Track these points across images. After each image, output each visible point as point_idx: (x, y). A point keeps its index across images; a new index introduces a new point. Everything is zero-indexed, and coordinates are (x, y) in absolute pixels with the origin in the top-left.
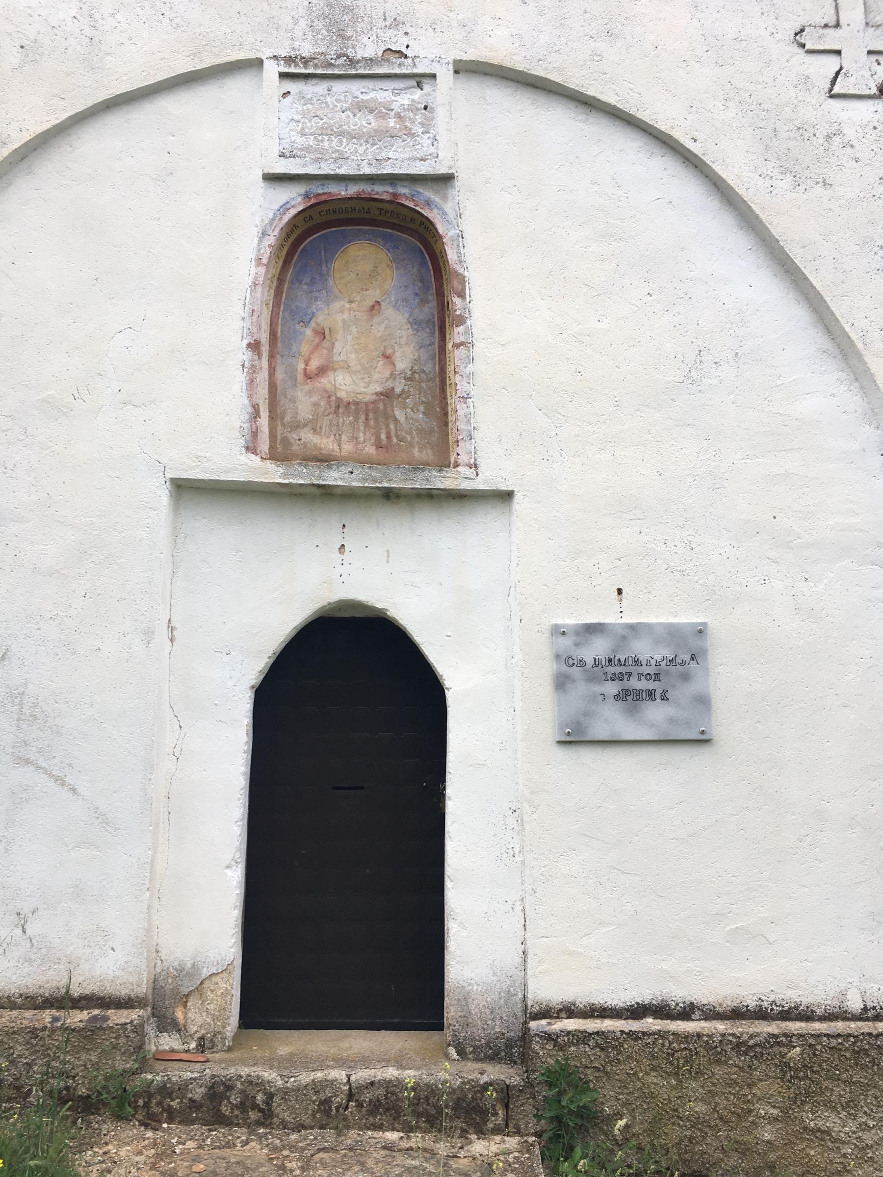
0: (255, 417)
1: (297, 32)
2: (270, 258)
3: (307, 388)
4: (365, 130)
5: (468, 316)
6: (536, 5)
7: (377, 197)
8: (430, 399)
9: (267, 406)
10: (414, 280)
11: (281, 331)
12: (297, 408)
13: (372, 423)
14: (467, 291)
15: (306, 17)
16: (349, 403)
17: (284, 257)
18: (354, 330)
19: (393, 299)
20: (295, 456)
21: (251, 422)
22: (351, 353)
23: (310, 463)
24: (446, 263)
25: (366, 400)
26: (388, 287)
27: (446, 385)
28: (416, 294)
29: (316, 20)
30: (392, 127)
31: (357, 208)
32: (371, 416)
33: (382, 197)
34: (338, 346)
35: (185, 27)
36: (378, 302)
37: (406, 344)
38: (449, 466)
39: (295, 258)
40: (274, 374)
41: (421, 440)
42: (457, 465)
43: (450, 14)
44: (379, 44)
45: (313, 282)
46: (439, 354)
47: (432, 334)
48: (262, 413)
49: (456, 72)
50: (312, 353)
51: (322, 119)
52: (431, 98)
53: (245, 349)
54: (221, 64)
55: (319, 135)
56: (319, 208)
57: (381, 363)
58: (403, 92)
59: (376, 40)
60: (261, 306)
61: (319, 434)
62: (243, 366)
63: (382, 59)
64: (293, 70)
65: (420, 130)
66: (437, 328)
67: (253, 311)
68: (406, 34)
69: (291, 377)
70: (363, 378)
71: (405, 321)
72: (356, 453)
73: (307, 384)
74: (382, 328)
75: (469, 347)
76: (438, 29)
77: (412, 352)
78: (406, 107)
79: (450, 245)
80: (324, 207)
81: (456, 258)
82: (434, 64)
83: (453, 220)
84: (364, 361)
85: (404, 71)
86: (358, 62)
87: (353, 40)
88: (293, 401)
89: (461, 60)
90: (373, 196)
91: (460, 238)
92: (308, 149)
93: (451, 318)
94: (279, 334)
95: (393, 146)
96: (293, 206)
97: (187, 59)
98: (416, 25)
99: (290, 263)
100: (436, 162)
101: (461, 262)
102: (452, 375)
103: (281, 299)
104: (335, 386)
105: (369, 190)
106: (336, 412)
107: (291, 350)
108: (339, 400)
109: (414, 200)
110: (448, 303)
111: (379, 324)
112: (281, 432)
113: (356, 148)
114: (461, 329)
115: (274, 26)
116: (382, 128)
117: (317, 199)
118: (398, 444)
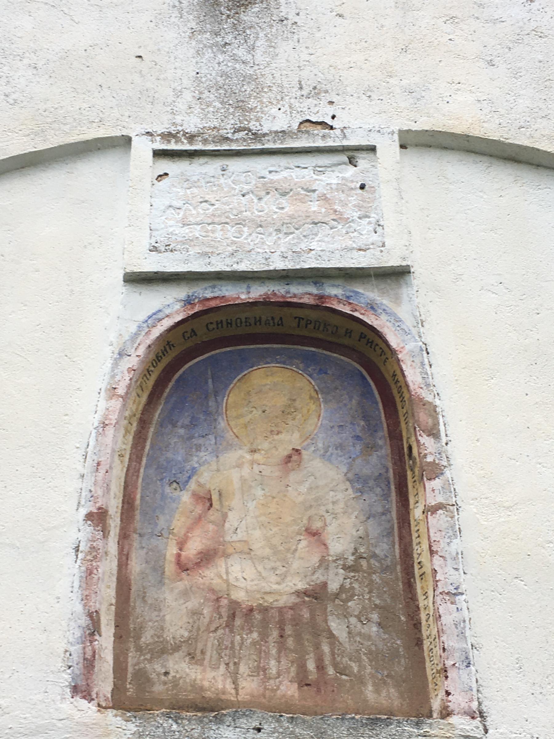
0: (92, 634)
1: (180, 105)
2: (129, 387)
3: (181, 585)
4: (275, 217)
5: (445, 464)
6: (509, 66)
7: (295, 300)
8: (389, 600)
9: (112, 617)
10: (353, 417)
11: (142, 497)
12: (163, 620)
13: (290, 642)
14: (442, 427)
15: (192, 89)
16: (251, 610)
17: (150, 388)
18: (259, 492)
19: (320, 445)
20: (158, 703)
21: (83, 642)
22: (254, 529)
23: (184, 714)
24: (404, 390)
25: (281, 604)
26: (313, 428)
27: (414, 577)
28: (358, 438)
29: (206, 91)
30: (314, 212)
31: (264, 318)
32: (289, 630)
33: (301, 301)
34: (233, 519)
35: (25, 103)
36: (297, 450)
37: (344, 513)
38: (430, 716)
39: (167, 390)
40: (127, 564)
41: (377, 671)
42: (446, 713)
43: (391, 81)
44: (294, 115)
45: (193, 424)
46: (400, 528)
47: (386, 496)
48: (103, 628)
49: (402, 147)
50: (190, 529)
51: (213, 205)
52: (370, 175)
53: (82, 522)
54: (73, 143)
55: (209, 224)
56: (206, 319)
57: (303, 543)
58: (329, 169)
59: (289, 110)
60: (112, 456)
61: (200, 662)
62: (77, 549)
63: (299, 131)
64: (173, 146)
65: (356, 215)
66: (393, 487)
67: (99, 464)
68: (331, 103)
69: (154, 569)
70: (274, 569)
71: (341, 477)
72: (264, 697)
73: (181, 580)
74: (303, 489)
75: (452, 512)
76: (374, 96)
77: (355, 526)
78: (334, 186)
79: (409, 363)
80: (214, 318)
81: (419, 379)
82: (372, 134)
83: (411, 328)
84: (276, 541)
85: (330, 143)
86: (265, 135)
87: (258, 112)
88: (157, 607)
89: (409, 131)
90: (289, 300)
91: (425, 352)
92: (189, 241)
93: (417, 470)
94: (138, 502)
95: (316, 235)
96: (167, 316)
97: (25, 139)
98: (344, 93)
99: (159, 398)
100: (382, 251)
101: (428, 385)
102: (425, 558)
103: (143, 448)
104: (227, 581)
105: (283, 291)
106: (229, 625)
107: (156, 525)
108: (234, 605)
109: (350, 304)
110: (410, 448)
111: (300, 483)
112: (135, 660)
113: (262, 239)
114: (436, 483)
115: (148, 100)
116: (300, 213)
117: (204, 305)
118: (336, 679)
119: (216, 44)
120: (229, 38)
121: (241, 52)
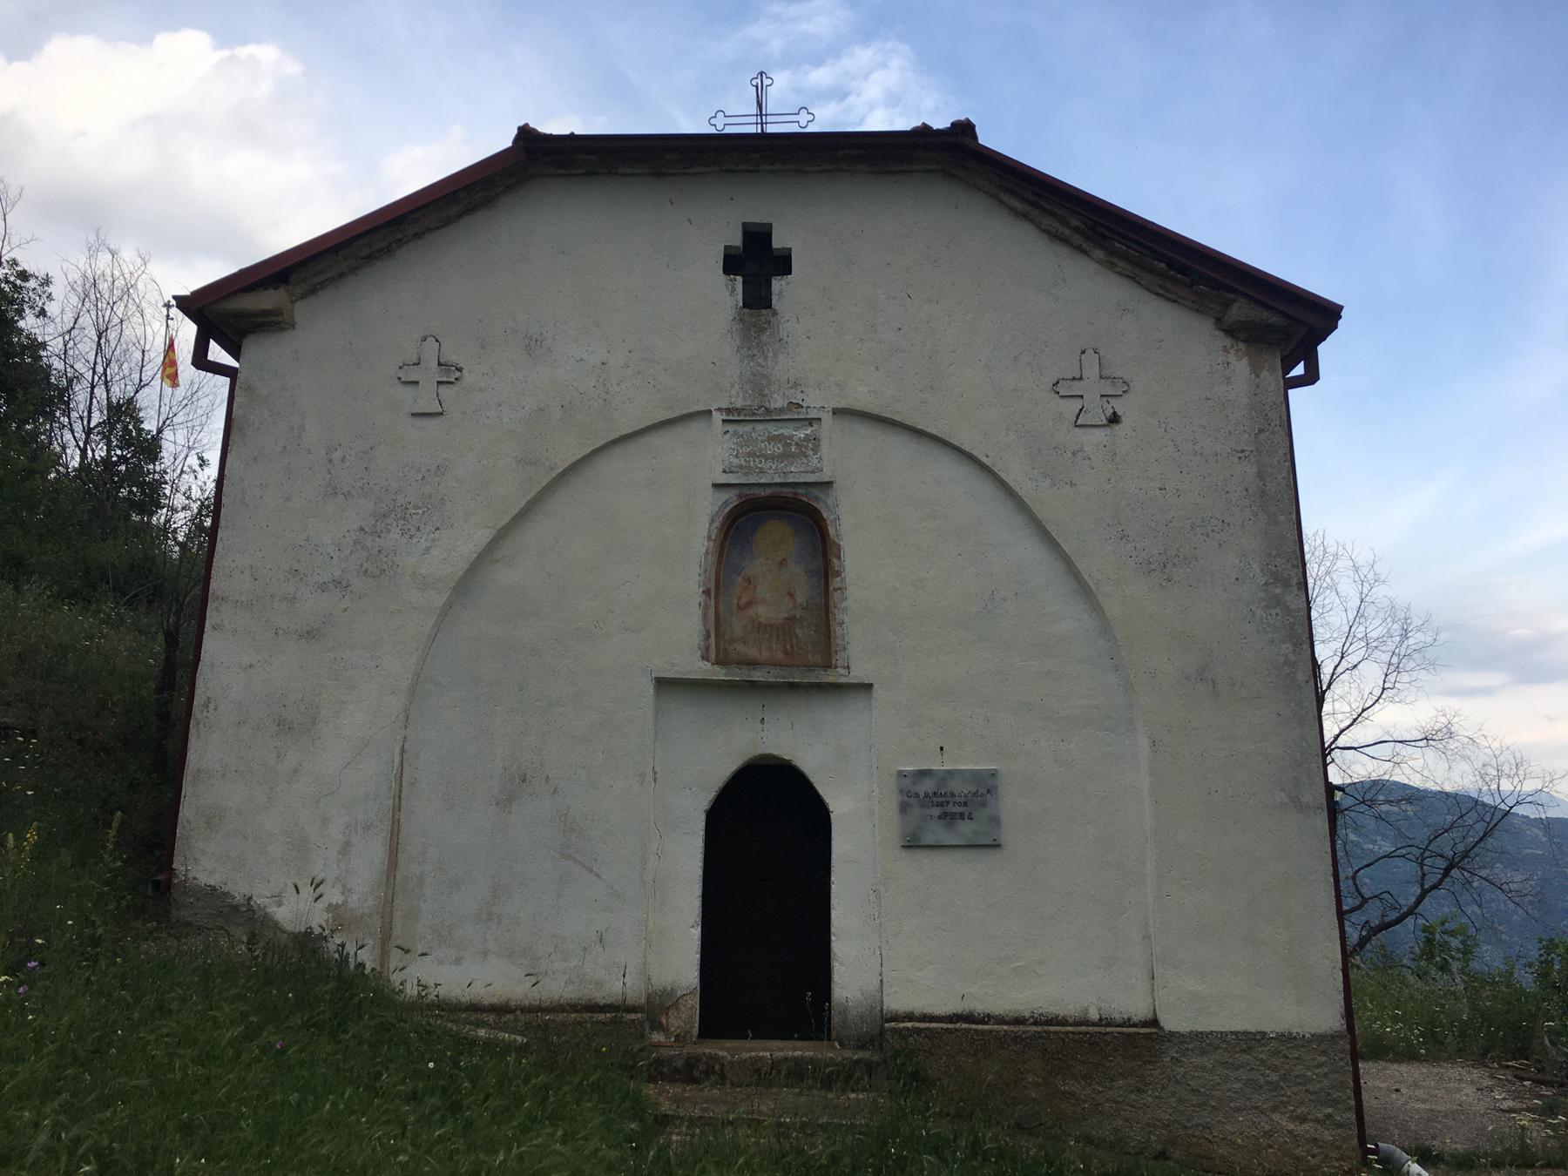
13: (781, 638)
38: (830, 667)
42: (836, 667)
57: (787, 599)
62: (700, 604)
68: (802, 392)
101: (838, 536)
106: (758, 631)
108: (760, 623)
114: (838, 579)
119: (749, 355)
120: (755, 352)
121: (761, 360)
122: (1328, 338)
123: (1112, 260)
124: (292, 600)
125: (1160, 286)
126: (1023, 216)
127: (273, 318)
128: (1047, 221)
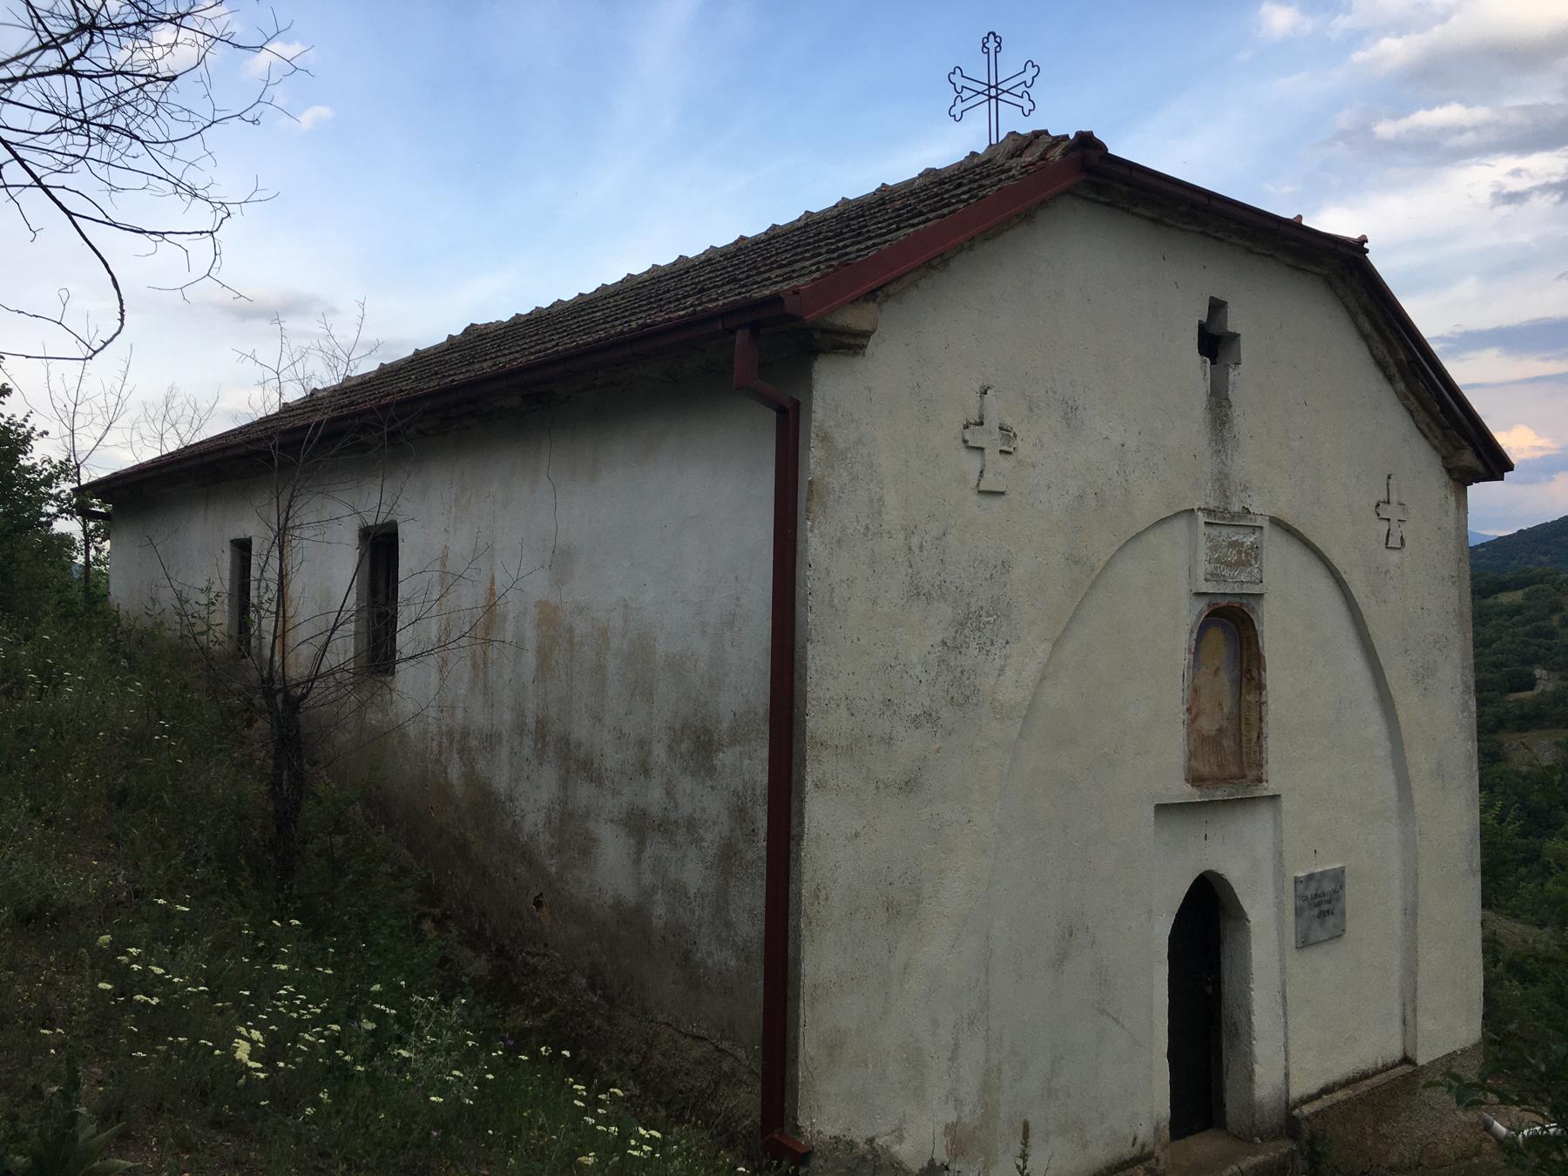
122: (1481, 483)
123: (1408, 394)
124: (888, 741)
125: (1428, 425)
126: (1365, 337)
127: (846, 340)
128: (1382, 350)
